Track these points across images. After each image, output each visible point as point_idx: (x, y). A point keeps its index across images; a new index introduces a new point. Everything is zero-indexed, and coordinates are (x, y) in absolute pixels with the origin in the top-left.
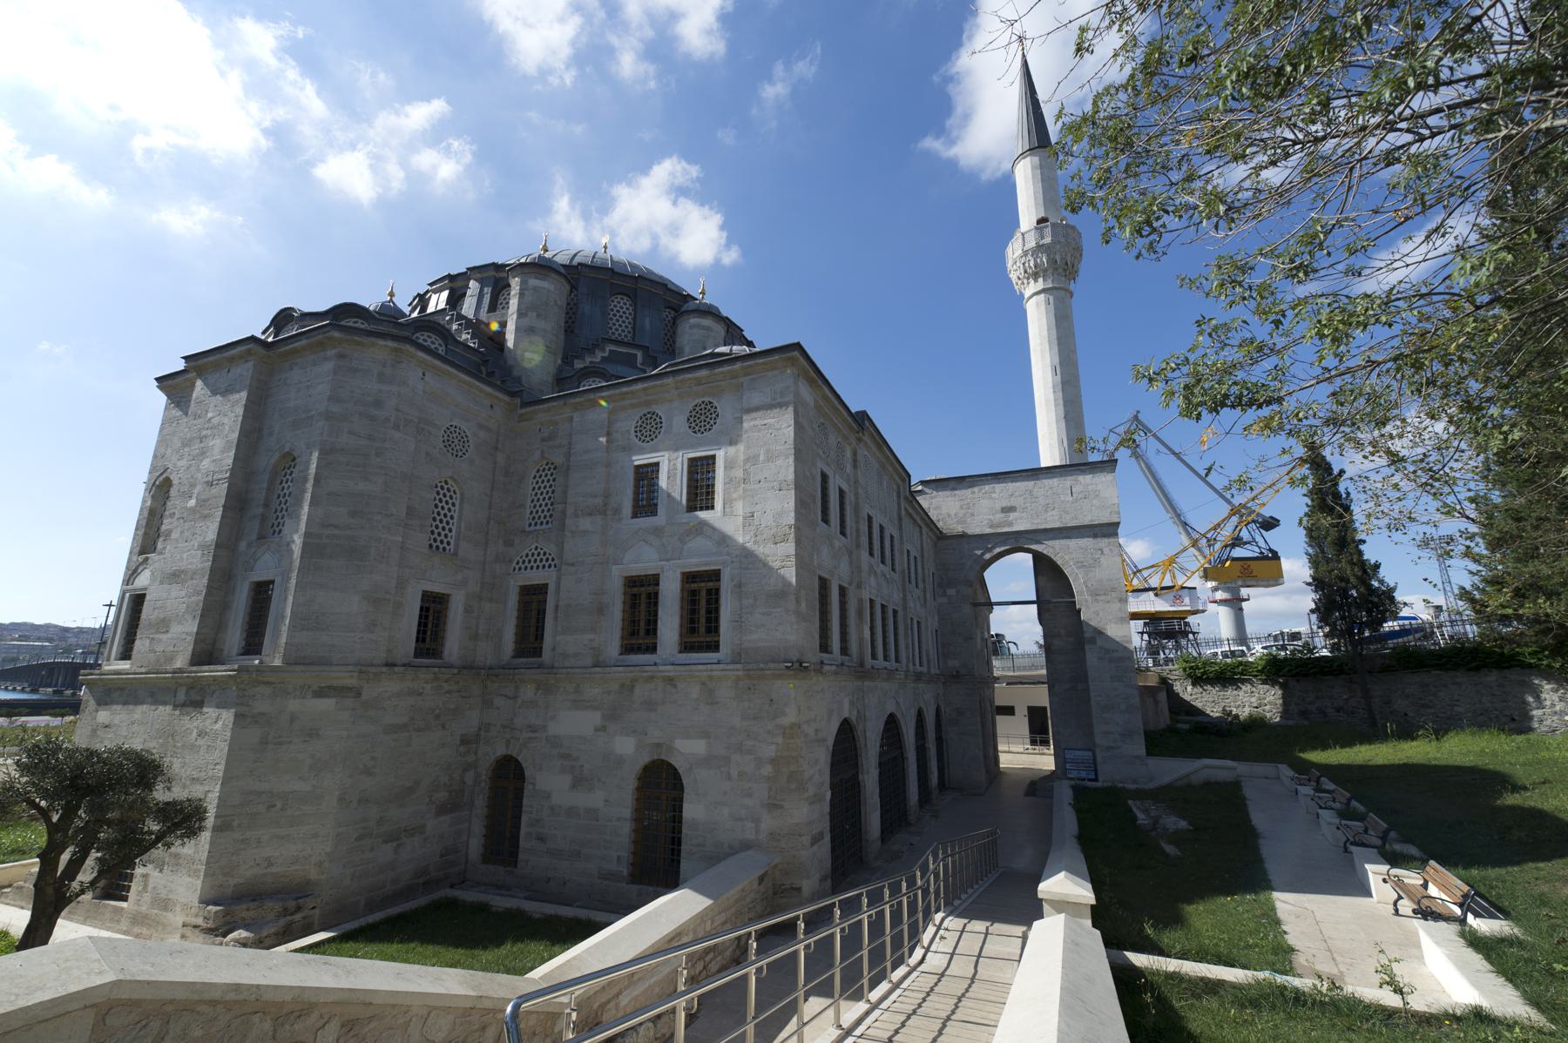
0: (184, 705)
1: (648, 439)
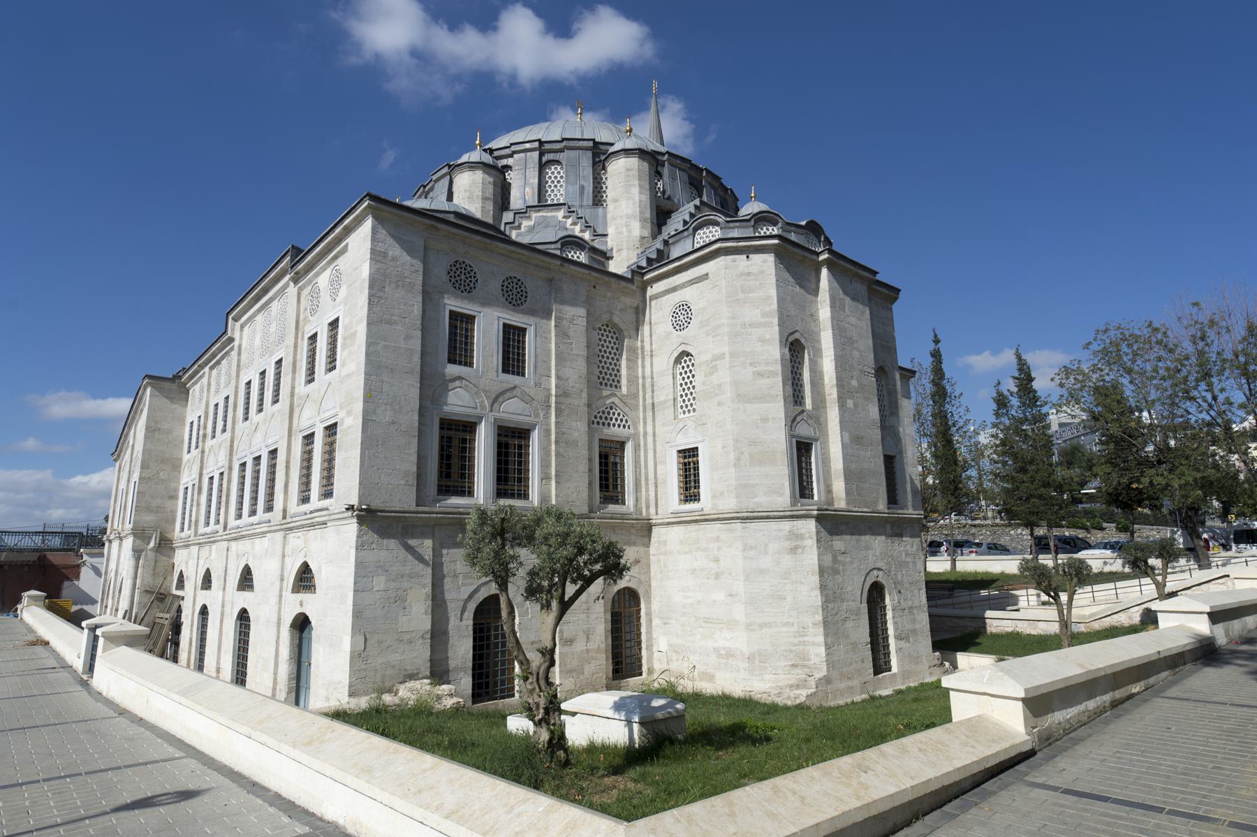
0: (892, 536)
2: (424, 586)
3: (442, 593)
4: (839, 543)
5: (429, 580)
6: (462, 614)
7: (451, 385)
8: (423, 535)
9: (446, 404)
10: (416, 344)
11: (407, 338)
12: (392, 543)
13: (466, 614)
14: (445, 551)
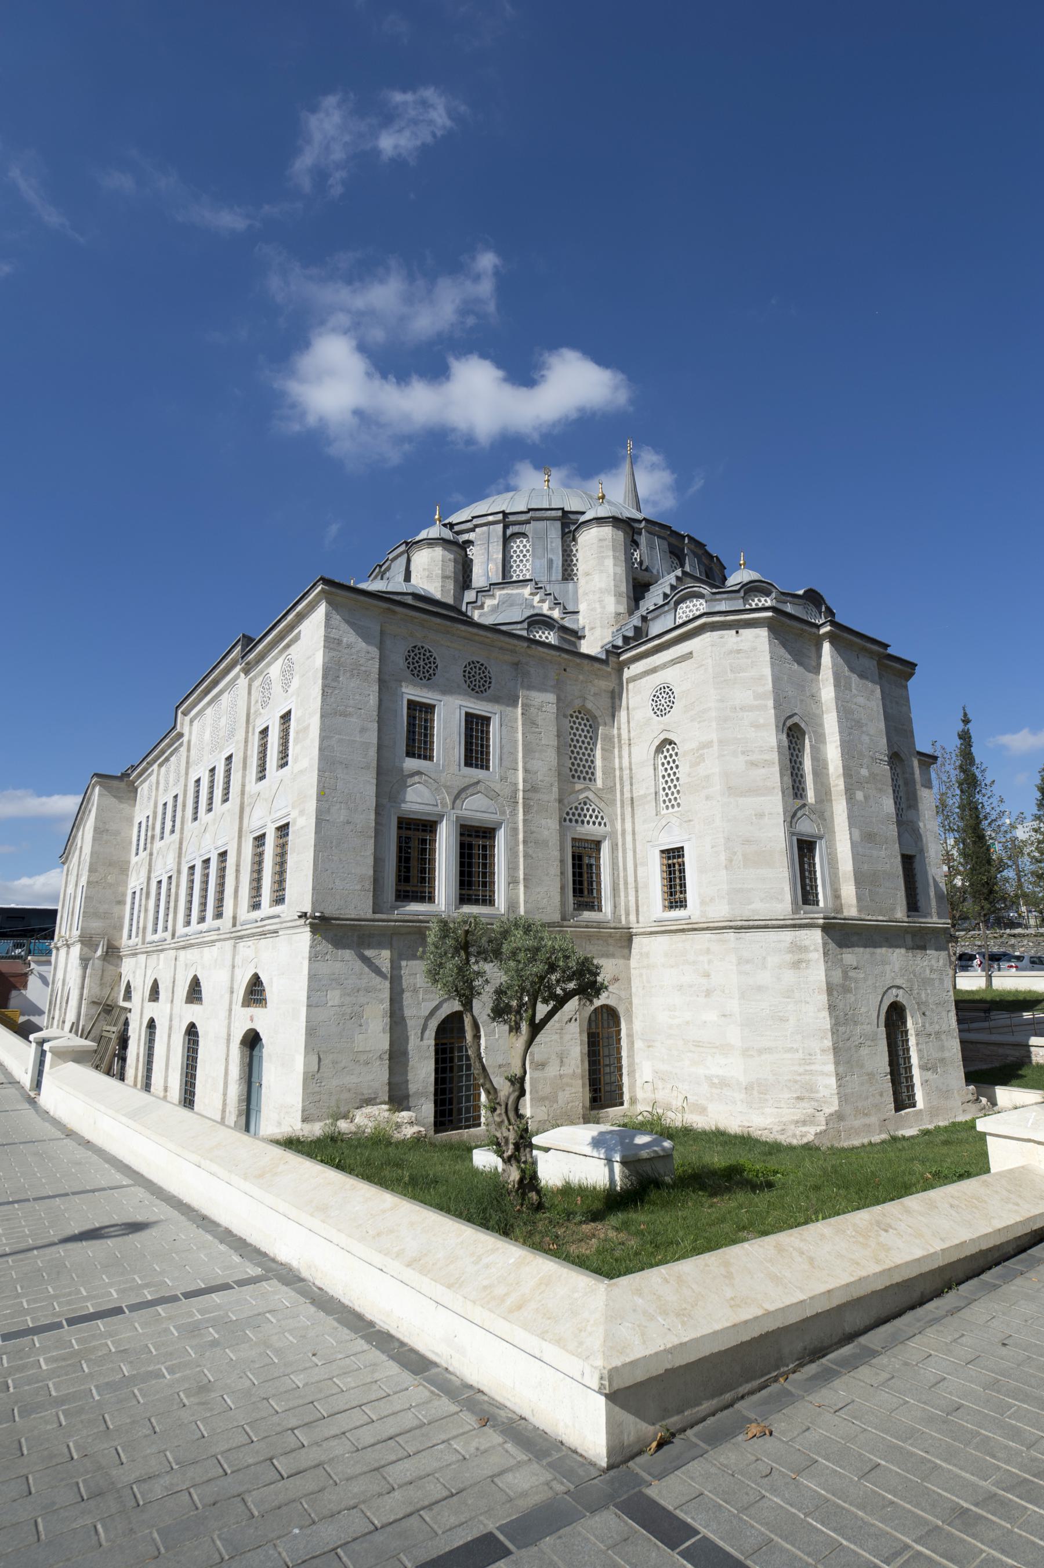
0: (913, 948)
1: (487, 685)
2: (381, 1001)
3: (401, 1009)
4: (850, 957)
5: (386, 995)
6: (423, 1033)
7: (410, 781)
8: (380, 946)
9: (404, 801)
10: (372, 737)
11: (363, 730)
12: (348, 954)
13: (427, 1033)
14: (404, 963)
